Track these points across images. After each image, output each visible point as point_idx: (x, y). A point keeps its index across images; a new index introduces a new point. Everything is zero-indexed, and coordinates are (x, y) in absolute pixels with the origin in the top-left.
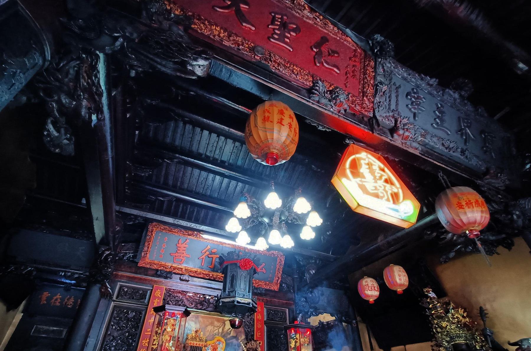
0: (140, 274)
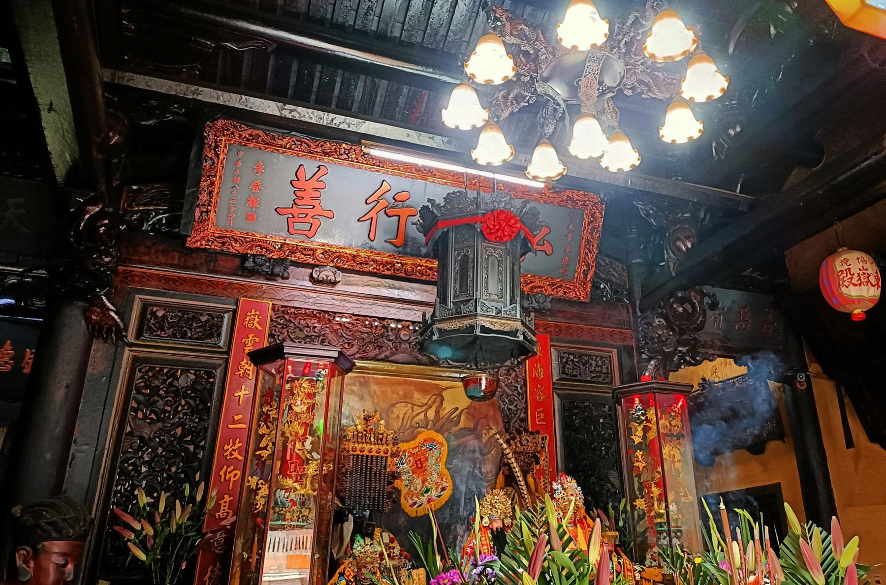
0: (195, 268)
